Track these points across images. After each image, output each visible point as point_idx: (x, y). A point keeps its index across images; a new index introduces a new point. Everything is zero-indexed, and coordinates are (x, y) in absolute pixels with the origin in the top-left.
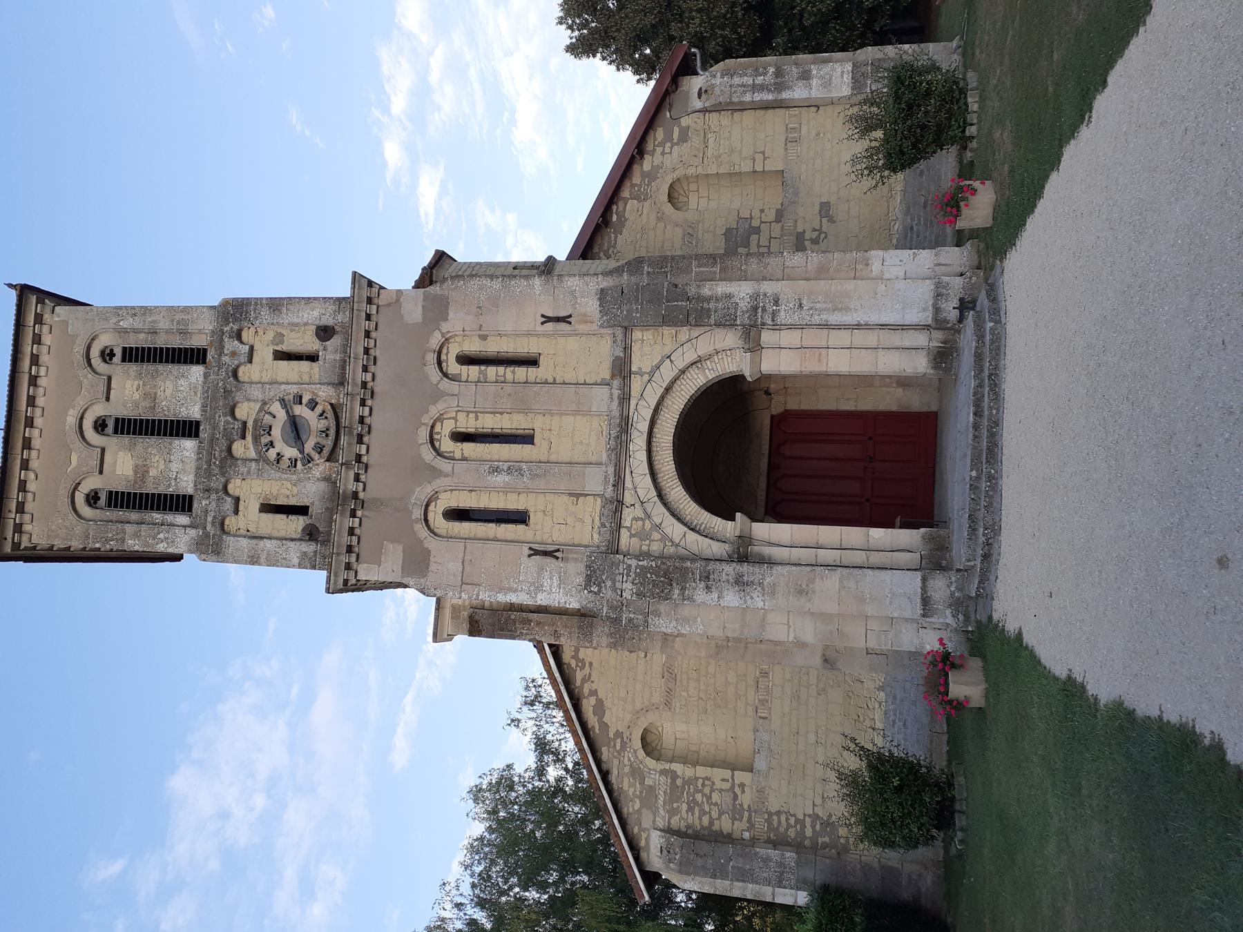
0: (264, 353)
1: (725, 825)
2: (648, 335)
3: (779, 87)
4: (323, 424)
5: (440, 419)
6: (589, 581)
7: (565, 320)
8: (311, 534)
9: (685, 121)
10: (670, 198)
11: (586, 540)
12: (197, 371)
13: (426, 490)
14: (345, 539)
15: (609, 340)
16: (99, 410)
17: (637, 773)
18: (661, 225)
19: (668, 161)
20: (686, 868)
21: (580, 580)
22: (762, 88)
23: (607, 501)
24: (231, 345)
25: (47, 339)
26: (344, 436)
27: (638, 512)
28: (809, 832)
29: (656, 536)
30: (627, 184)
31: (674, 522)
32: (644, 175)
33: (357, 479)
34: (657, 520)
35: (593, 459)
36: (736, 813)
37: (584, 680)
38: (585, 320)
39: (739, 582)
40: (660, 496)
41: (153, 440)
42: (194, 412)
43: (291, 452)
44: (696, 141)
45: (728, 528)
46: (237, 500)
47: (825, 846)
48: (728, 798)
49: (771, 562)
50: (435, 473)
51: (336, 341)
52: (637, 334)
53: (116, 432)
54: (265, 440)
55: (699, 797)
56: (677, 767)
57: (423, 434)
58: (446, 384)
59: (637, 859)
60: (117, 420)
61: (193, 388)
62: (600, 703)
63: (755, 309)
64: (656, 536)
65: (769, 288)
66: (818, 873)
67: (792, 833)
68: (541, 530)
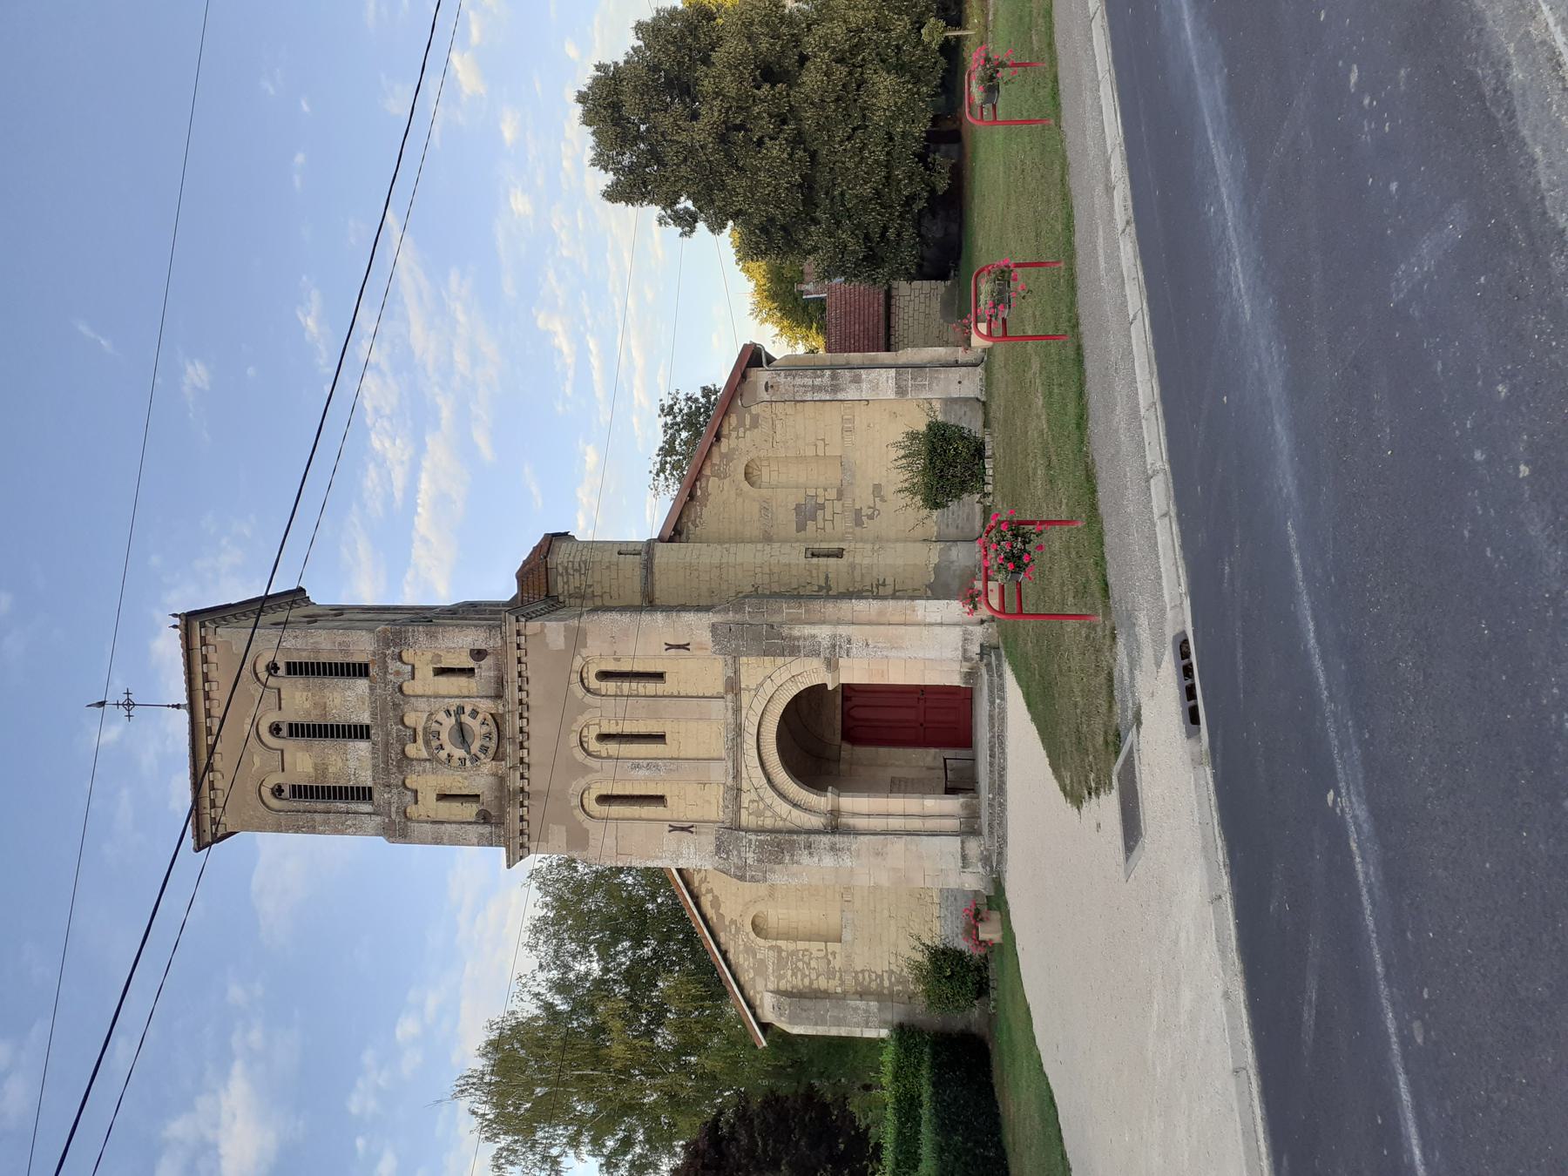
0: (425, 671)
1: (822, 983)
2: (752, 660)
3: (835, 389)
4: (485, 729)
5: (587, 726)
6: (718, 849)
7: (685, 647)
8: (484, 818)
9: (755, 409)
10: (747, 476)
11: (714, 817)
12: (362, 684)
13: (582, 783)
14: (518, 825)
15: (722, 663)
16: (273, 717)
17: (751, 951)
18: (740, 500)
19: (742, 444)
20: (793, 1020)
21: (712, 848)
22: (820, 389)
23: (728, 789)
24: (393, 666)
25: (213, 657)
26: (504, 739)
27: (754, 796)
28: (886, 983)
29: (768, 813)
30: (708, 463)
31: (784, 802)
32: (723, 456)
33: (522, 777)
34: (769, 802)
35: (715, 755)
36: (830, 974)
37: (701, 882)
38: (701, 647)
39: (833, 848)
40: (769, 781)
41: (328, 742)
42: (365, 718)
43: (459, 753)
44: (765, 427)
45: (823, 802)
46: (416, 792)
47: (899, 992)
48: (822, 965)
49: (857, 833)
50: (587, 770)
51: (487, 662)
52: (744, 660)
53: (291, 735)
54: (435, 743)
55: (800, 964)
56: (781, 943)
57: (574, 739)
58: (589, 698)
59: (754, 1015)
60: (290, 725)
61: (361, 698)
62: (716, 898)
63: (834, 646)
64: (768, 813)
65: (843, 630)
66: (896, 1014)
67: (874, 985)
68: (678, 808)
